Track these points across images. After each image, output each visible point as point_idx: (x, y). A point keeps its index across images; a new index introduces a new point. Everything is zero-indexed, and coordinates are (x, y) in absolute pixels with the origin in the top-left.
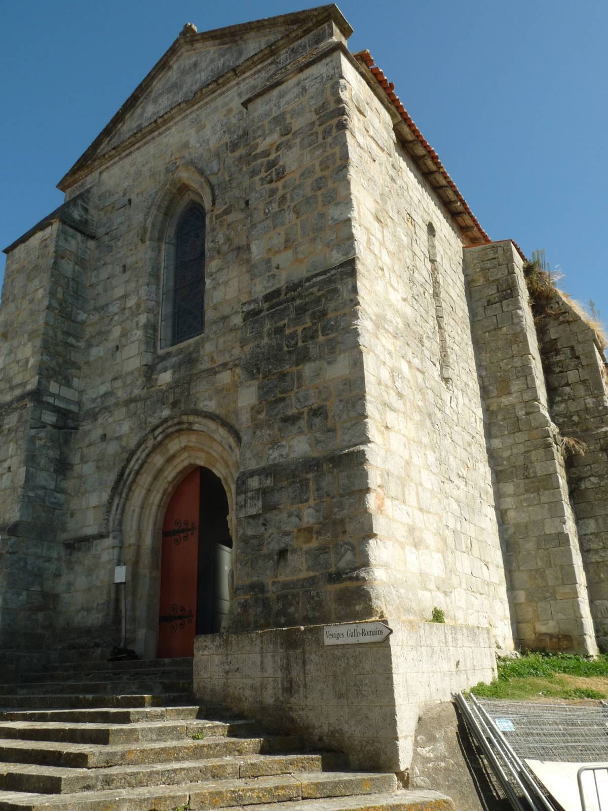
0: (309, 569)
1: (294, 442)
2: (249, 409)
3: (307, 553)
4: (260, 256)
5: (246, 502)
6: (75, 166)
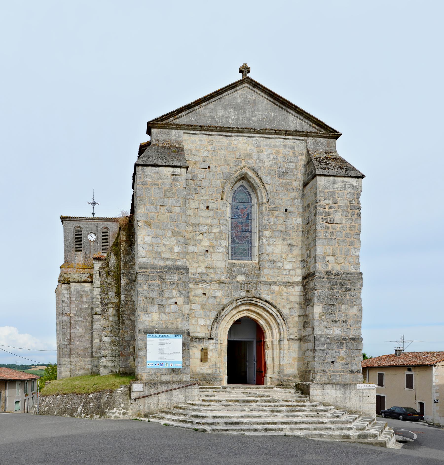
0: (342, 368)
1: (335, 329)
2: (319, 314)
3: (341, 364)
4: (321, 254)
5: (319, 345)
6: (164, 116)
